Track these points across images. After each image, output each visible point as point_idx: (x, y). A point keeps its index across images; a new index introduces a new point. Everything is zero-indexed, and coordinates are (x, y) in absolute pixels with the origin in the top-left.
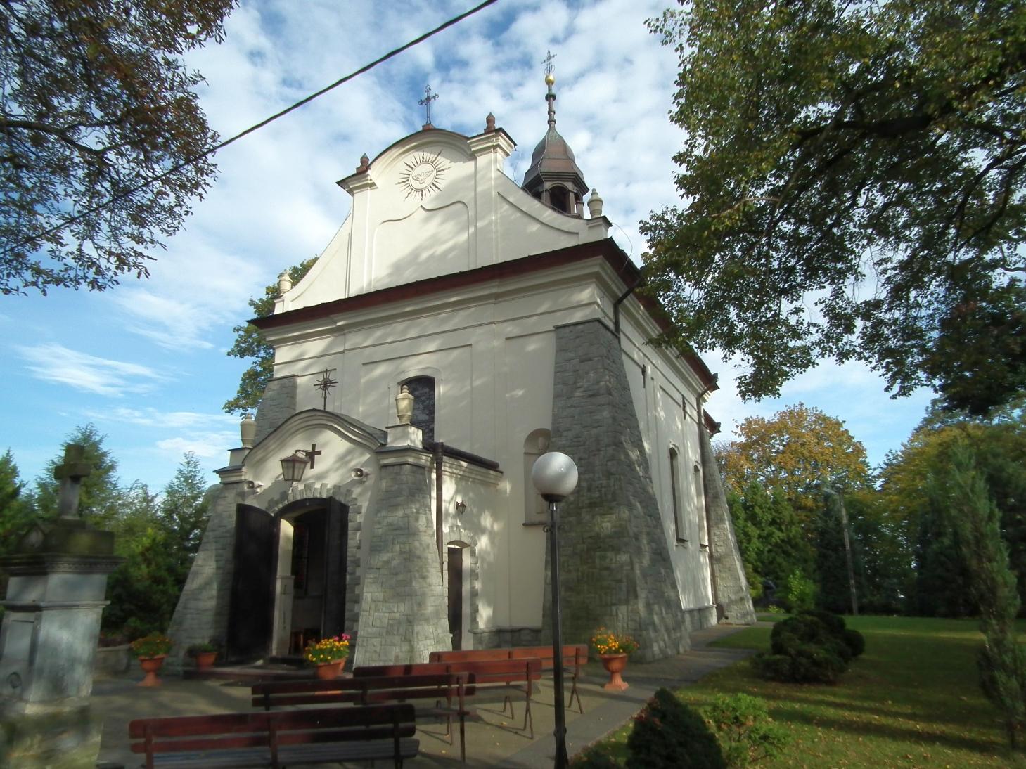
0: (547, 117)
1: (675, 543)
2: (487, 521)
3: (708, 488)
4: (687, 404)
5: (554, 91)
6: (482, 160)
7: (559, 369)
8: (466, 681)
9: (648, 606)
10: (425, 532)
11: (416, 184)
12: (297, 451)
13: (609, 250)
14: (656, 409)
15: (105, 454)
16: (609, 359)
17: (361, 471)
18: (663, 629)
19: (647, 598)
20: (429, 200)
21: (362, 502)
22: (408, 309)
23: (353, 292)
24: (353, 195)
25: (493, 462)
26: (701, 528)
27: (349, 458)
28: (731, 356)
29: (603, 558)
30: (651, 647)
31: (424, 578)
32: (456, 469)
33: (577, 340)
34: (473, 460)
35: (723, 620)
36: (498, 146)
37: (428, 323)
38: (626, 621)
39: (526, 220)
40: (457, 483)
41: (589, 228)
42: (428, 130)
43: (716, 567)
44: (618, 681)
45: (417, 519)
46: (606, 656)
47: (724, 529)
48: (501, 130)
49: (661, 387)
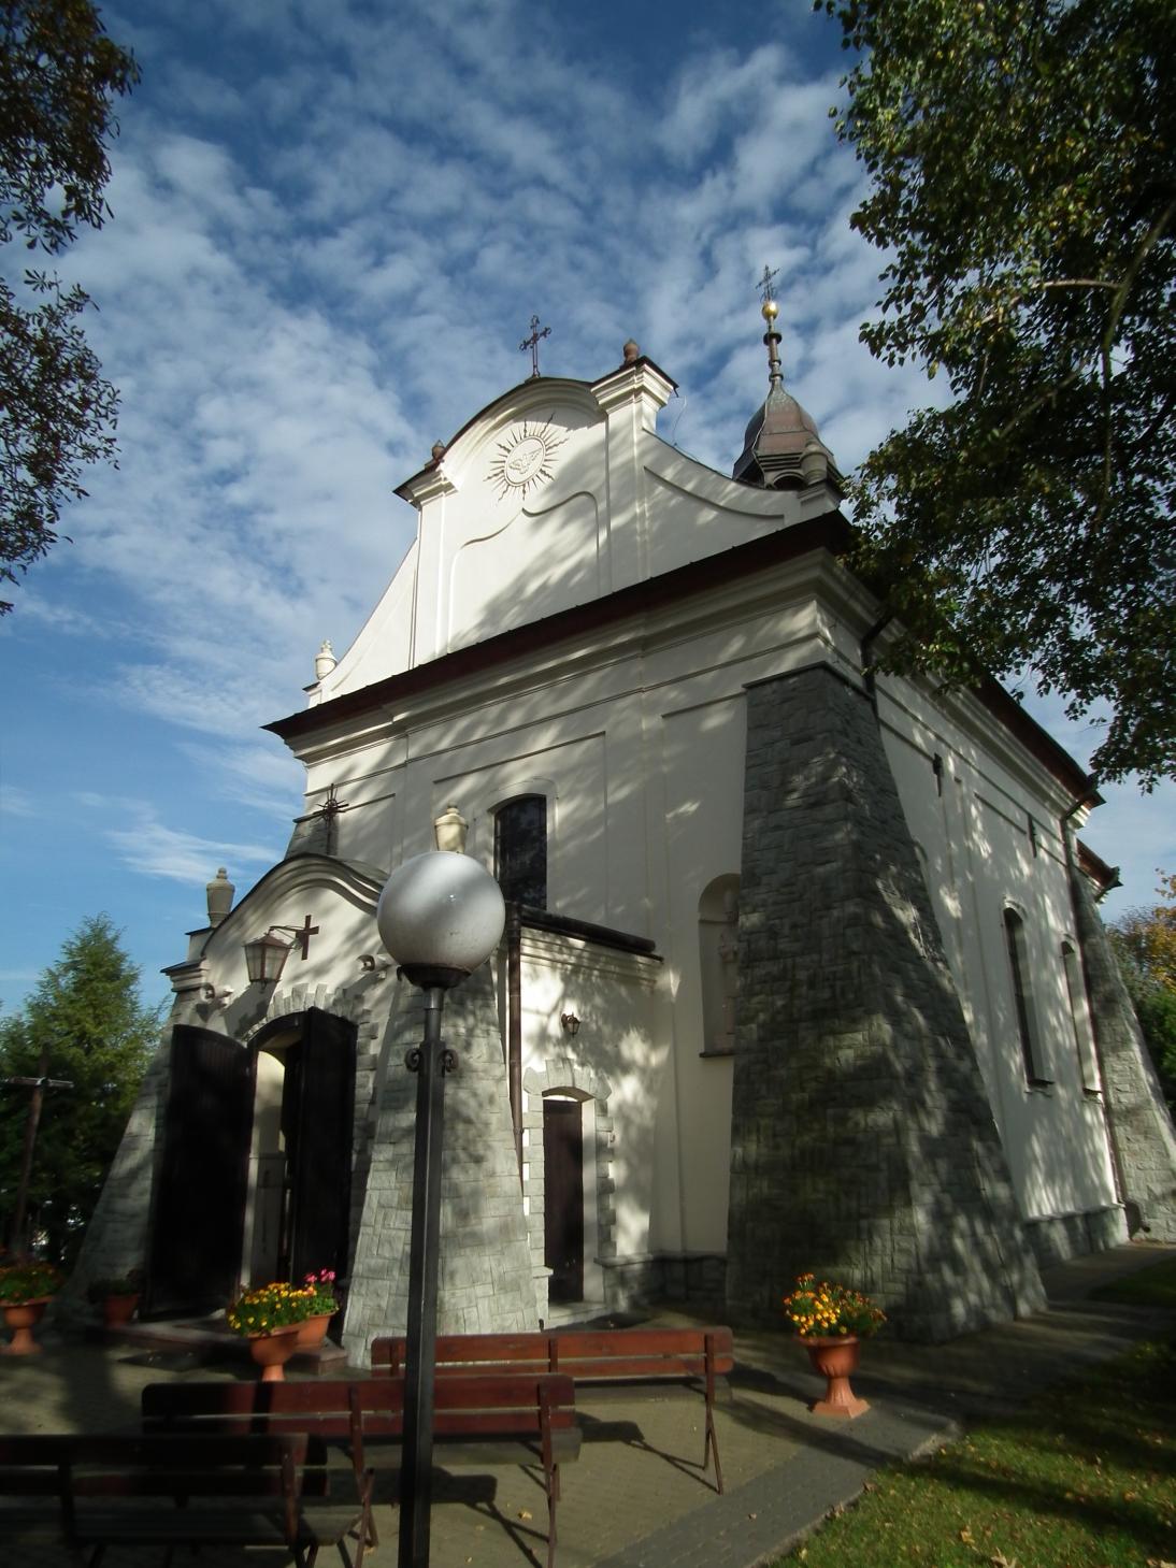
1: (1026, 1087)
2: (634, 1047)
3: (1092, 980)
4: (1038, 829)
6: (616, 417)
7: (754, 760)
8: (303, 1455)
9: (940, 1216)
10: (485, 1071)
11: (515, 476)
12: (272, 928)
13: (831, 533)
14: (969, 836)
15: (121, 958)
16: (847, 736)
17: (371, 959)
18: (977, 1266)
19: (938, 1202)
20: (537, 500)
21: (378, 1011)
22: (503, 681)
23: (423, 658)
25: (647, 941)
26: (1081, 1053)
27: (363, 934)
28: (1085, 707)
29: (841, 1120)
30: (948, 1308)
31: (478, 1160)
32: (561, 952)
33: (786, 706)
34: (598, 936)
35: (1141, 1235)
36: (643, 389)
37: (541, 700)
38: (888, 1252)
39: (694, 504)
40: (566, 979)
41: (803, 503)
42: (534, 382)
43: (1120, 1131)
44: (844, 1396)
45: (468, 1046)
46: (812, 1341)
47: (1131, 1060)
49: (977, 796)
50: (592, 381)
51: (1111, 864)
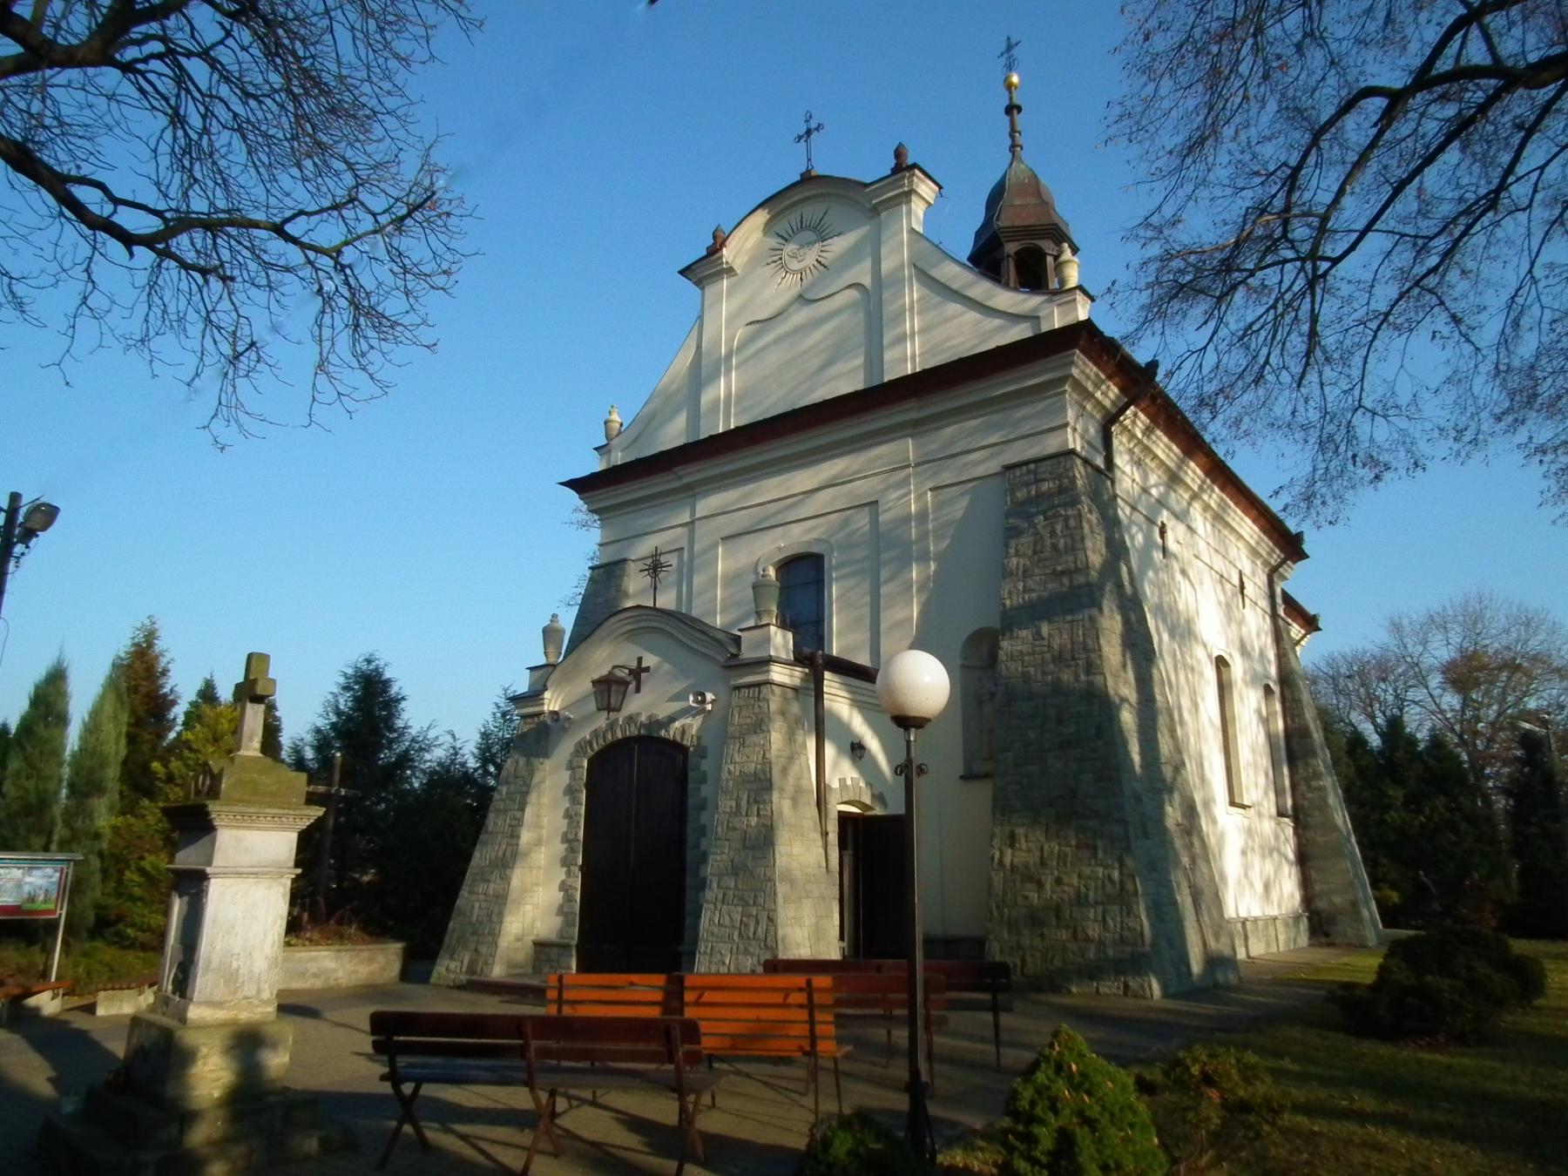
0: (1009, 142)
5: (1016, 101)
24: (702, 288)
42: (807, 178)
48: (915, 166)
50: (868, 181)
51: (1311, 611)
